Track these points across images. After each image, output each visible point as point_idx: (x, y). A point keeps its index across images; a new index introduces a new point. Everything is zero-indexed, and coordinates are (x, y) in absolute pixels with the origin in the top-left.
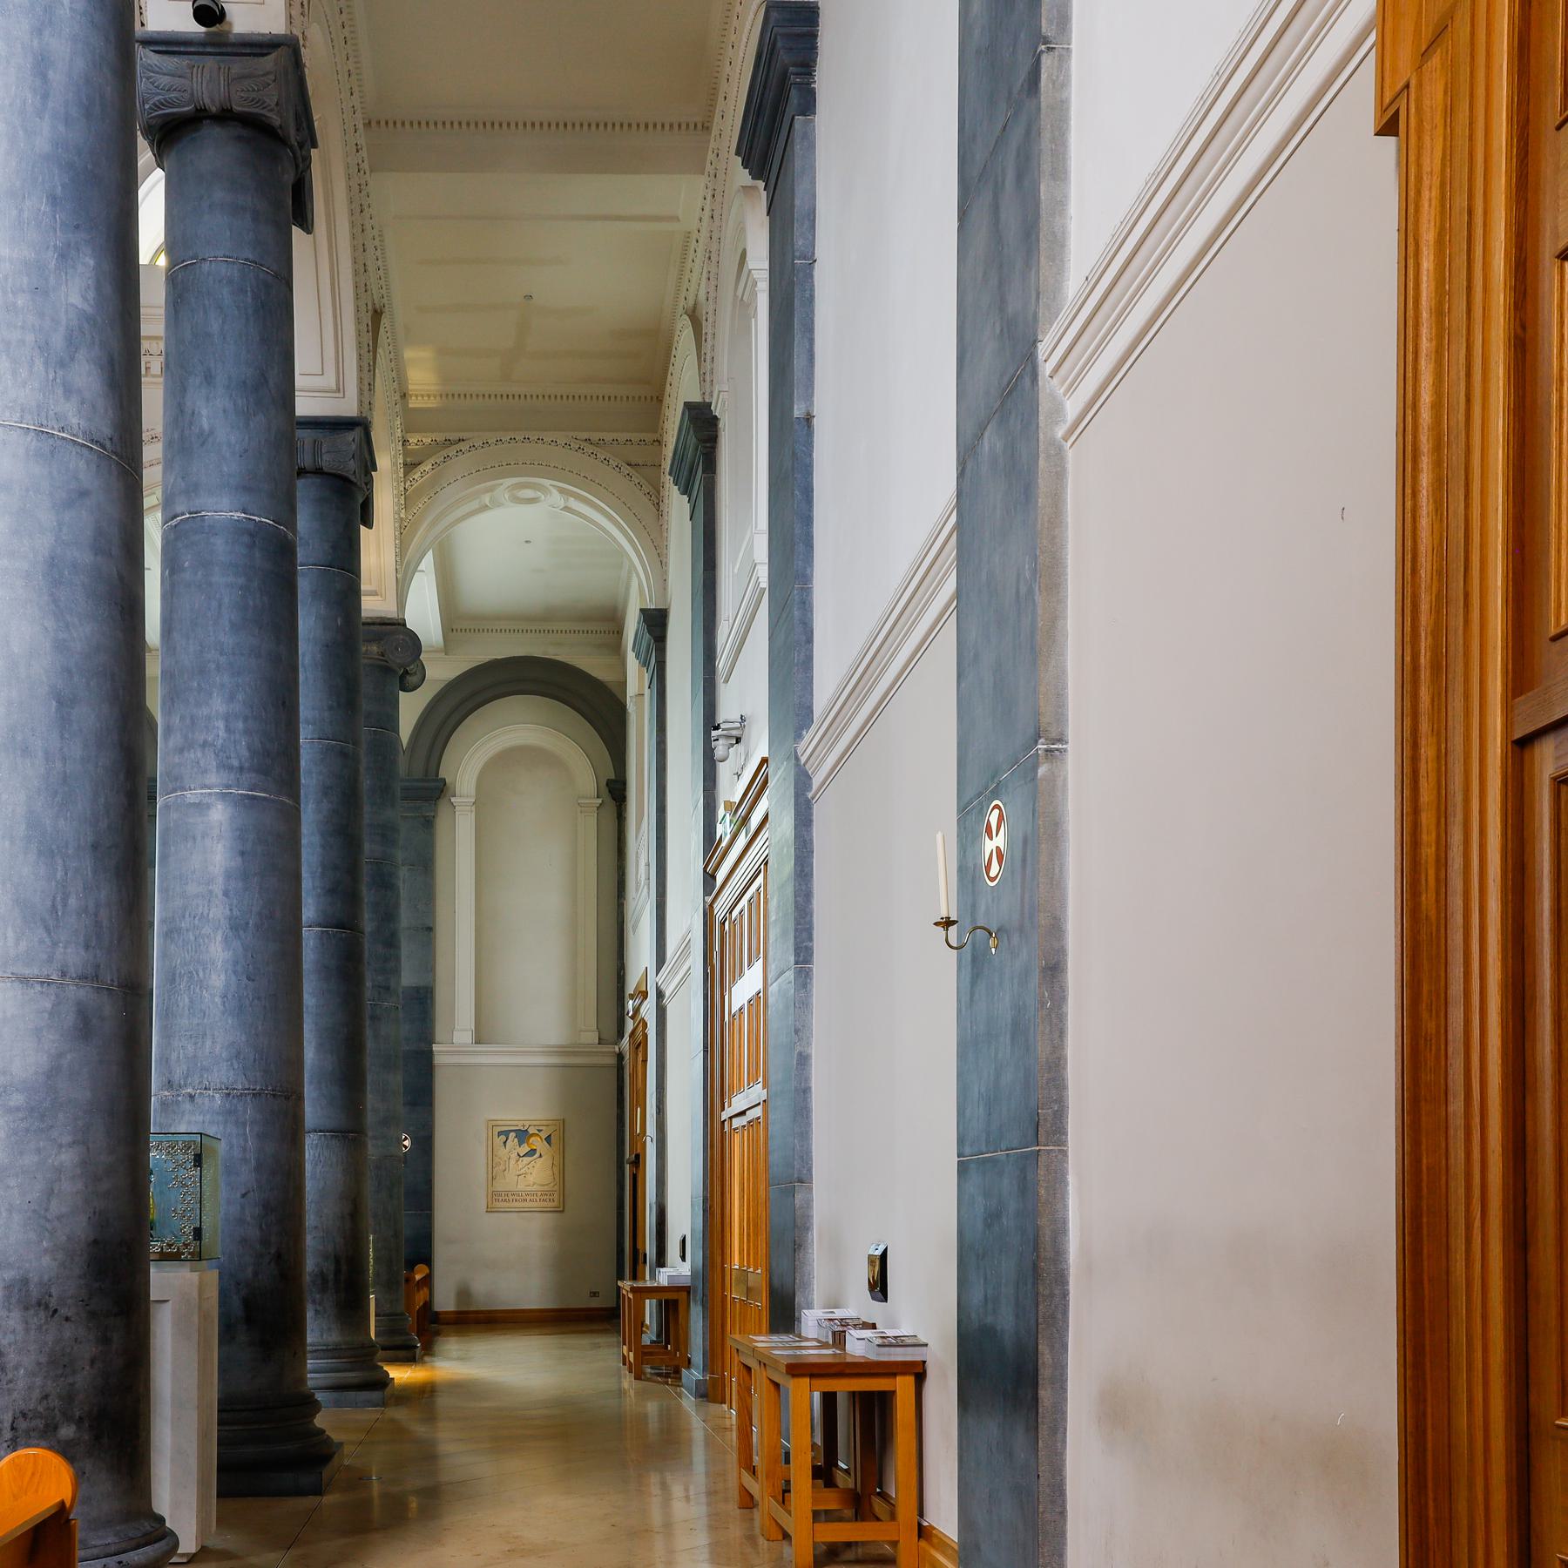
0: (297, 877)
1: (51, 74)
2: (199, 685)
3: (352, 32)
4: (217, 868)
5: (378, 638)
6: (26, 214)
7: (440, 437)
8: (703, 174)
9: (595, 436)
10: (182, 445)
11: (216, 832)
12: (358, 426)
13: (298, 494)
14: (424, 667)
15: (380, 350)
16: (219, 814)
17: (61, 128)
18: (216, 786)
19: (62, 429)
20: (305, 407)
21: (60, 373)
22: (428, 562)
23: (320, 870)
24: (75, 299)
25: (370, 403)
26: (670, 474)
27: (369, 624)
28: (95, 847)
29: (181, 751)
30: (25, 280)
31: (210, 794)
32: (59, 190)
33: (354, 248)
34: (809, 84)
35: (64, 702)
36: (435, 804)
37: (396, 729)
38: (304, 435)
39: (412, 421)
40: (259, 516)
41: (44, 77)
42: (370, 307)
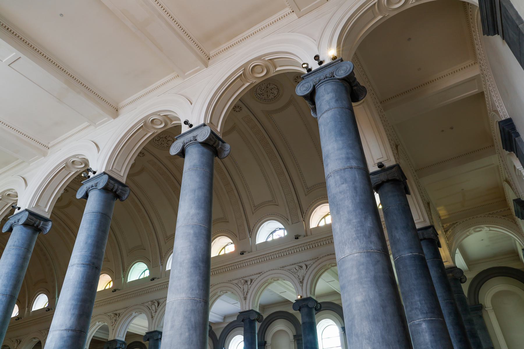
0: (450, 339)
1: (357, 189)
2: (411, 294)
3: (370, 83)
4: (428, 340)
5: (451, 272)
6: (357, 213)
7: (451, 223)
8: (496, 154)
9: (491, 212)
10: (394, 243)
11: (425, 330)
12: (432, 227)
13: (422, 245)
14: (465, 276)
15: (431, 210)
16: (424, 326)
17: (361, 197)
18: (422, 319)
19: (372, 250)
20: (418, 226)
21: (369, 239)
22: (458, 251)
23: (455, 336)
24: (369, 225)
25: (432, 222)
26: (504, 149)
27: (447, 269)
28: (399, 341)
29: (411, 311)
30: (359, 224)
31: (421, 321)
32: (362, 207)
33: (420, 193)
34: (516, 131)
35: (384, 307)
36: (481, 311)
37: (463, 294)
38: (420, 232)
39: (443, 222)
40: (415, 253)
41: (356, 190)
42: (426, 202)
